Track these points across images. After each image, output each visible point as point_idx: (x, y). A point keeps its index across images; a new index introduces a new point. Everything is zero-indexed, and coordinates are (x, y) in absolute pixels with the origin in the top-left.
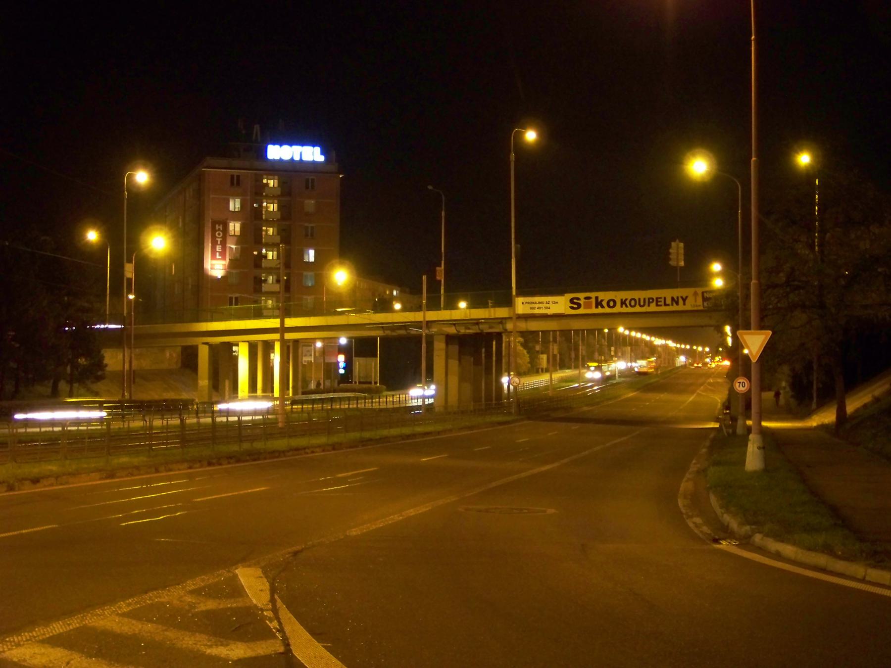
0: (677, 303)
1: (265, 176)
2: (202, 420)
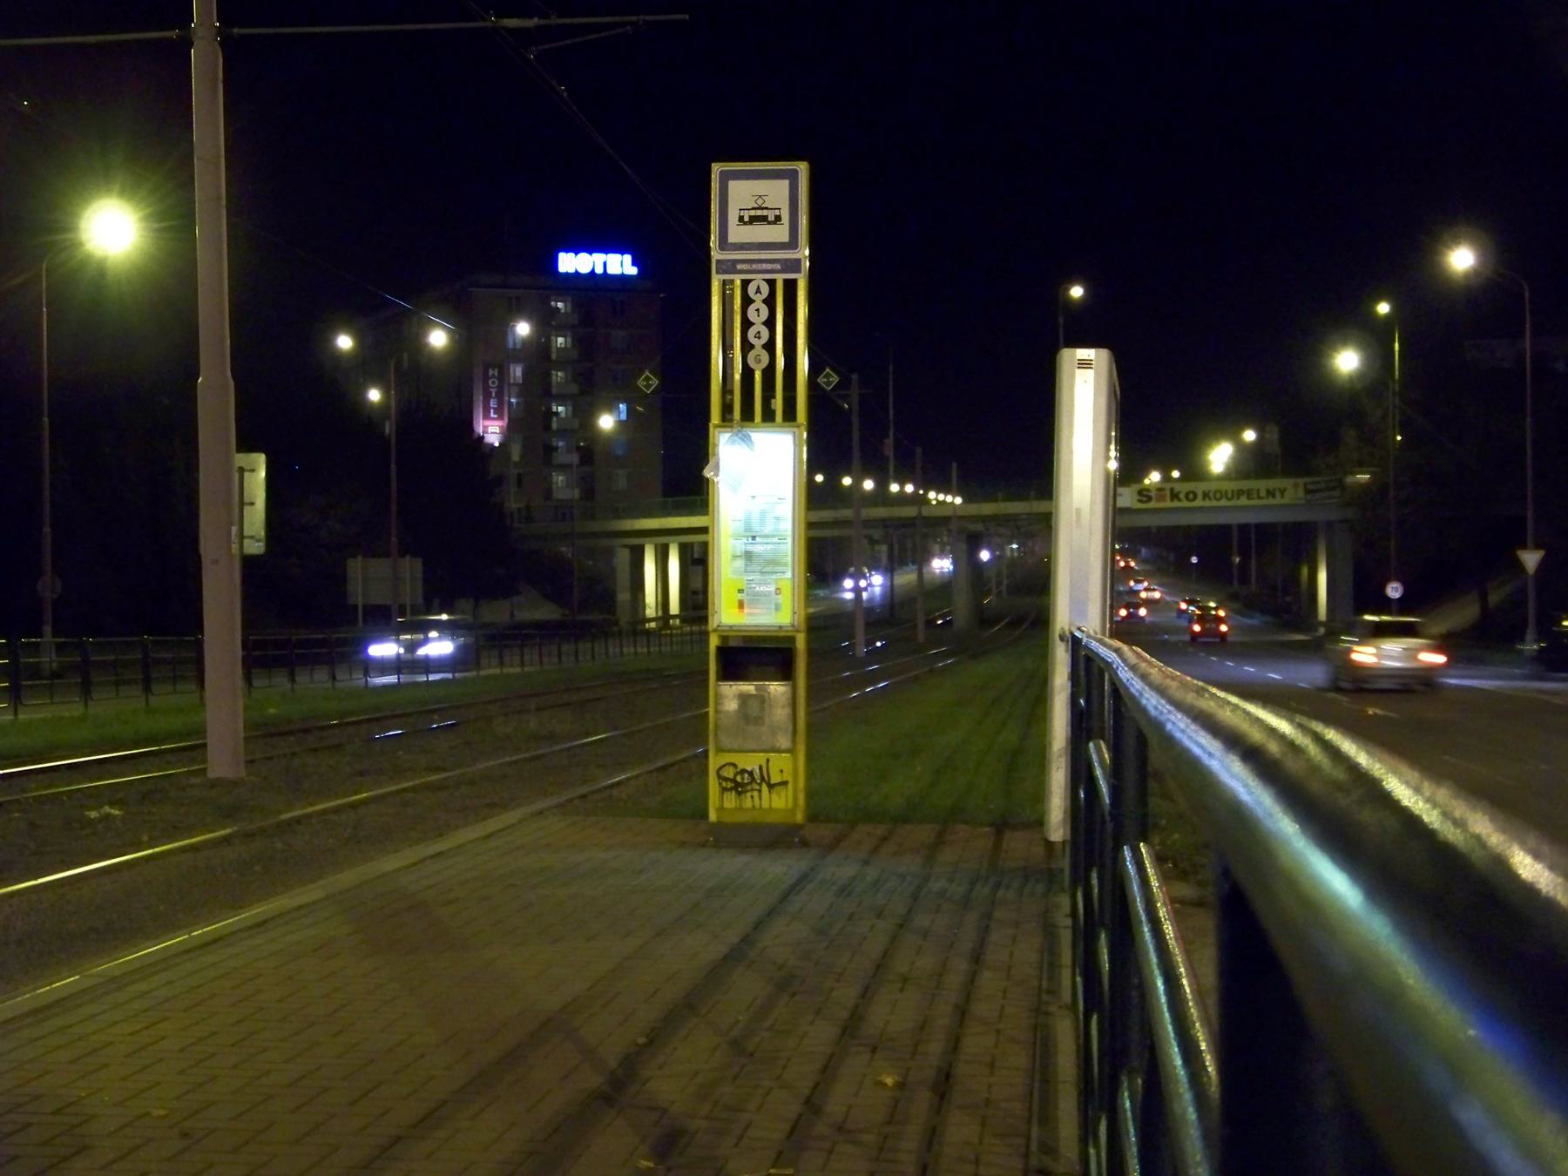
0: (1274, 496)
1: (553, 297)
2: (689, 629)
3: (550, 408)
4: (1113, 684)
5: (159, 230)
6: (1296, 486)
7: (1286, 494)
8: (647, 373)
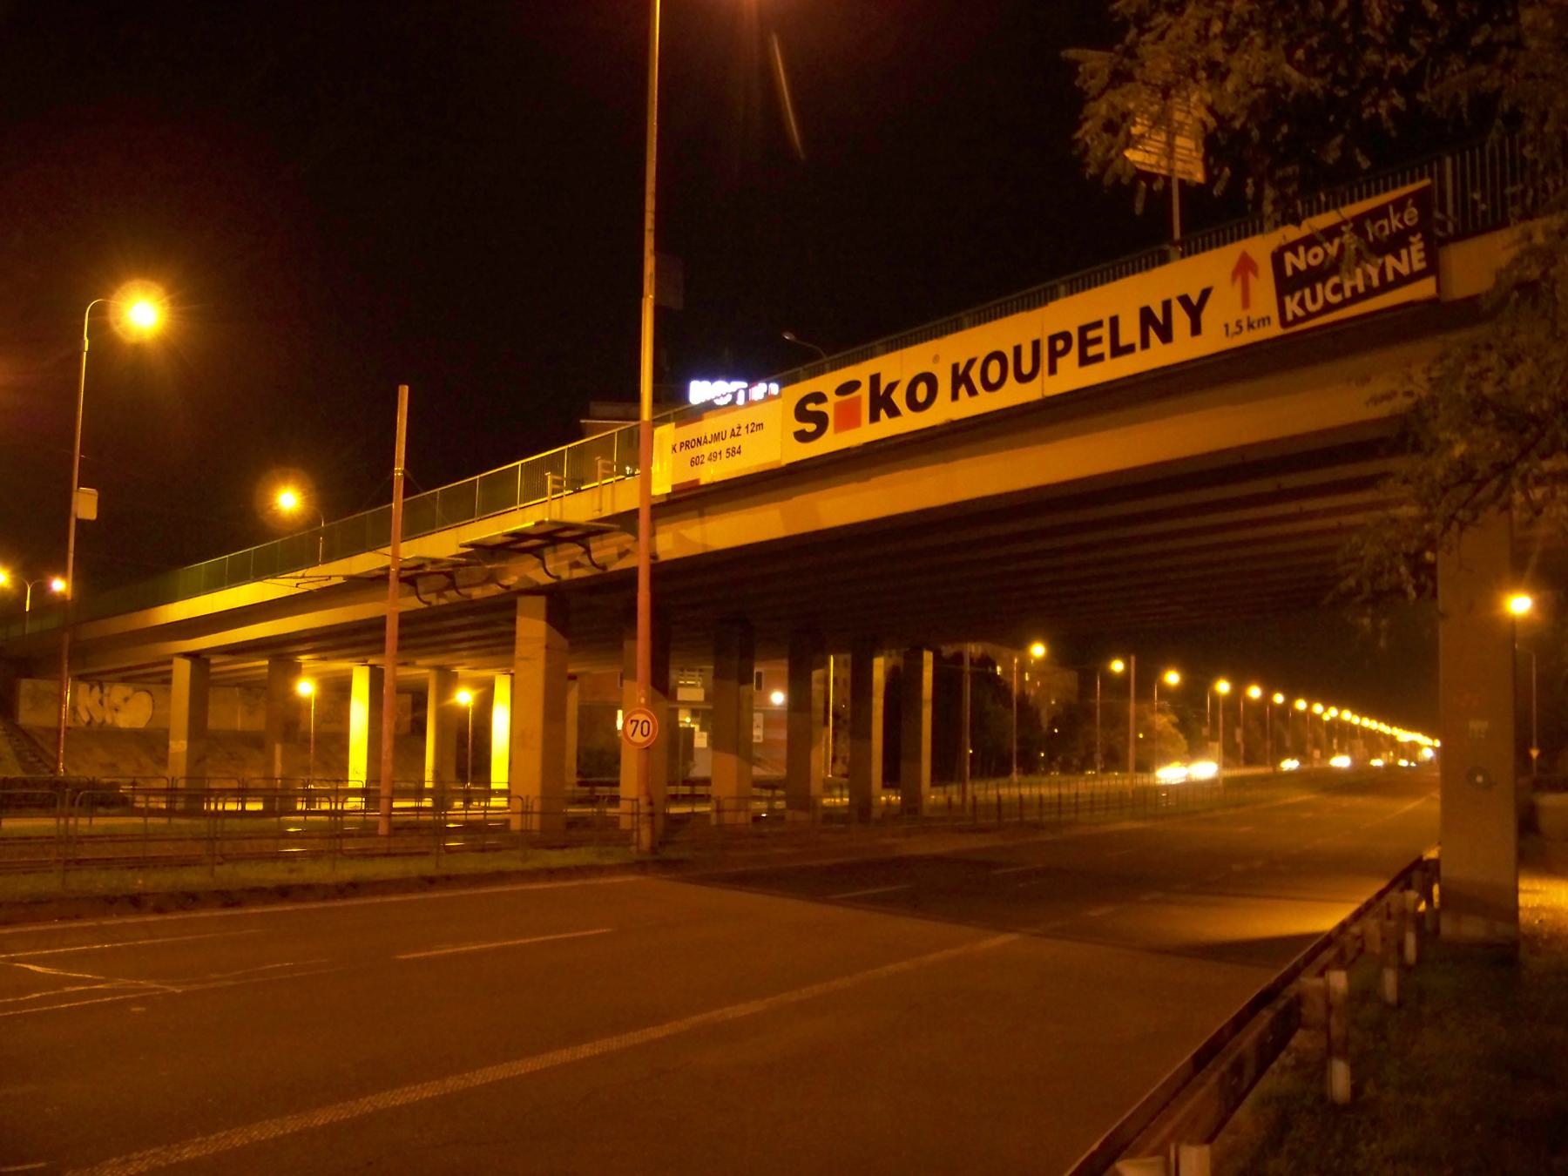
0: (1166, 335)
4: (449, 567)
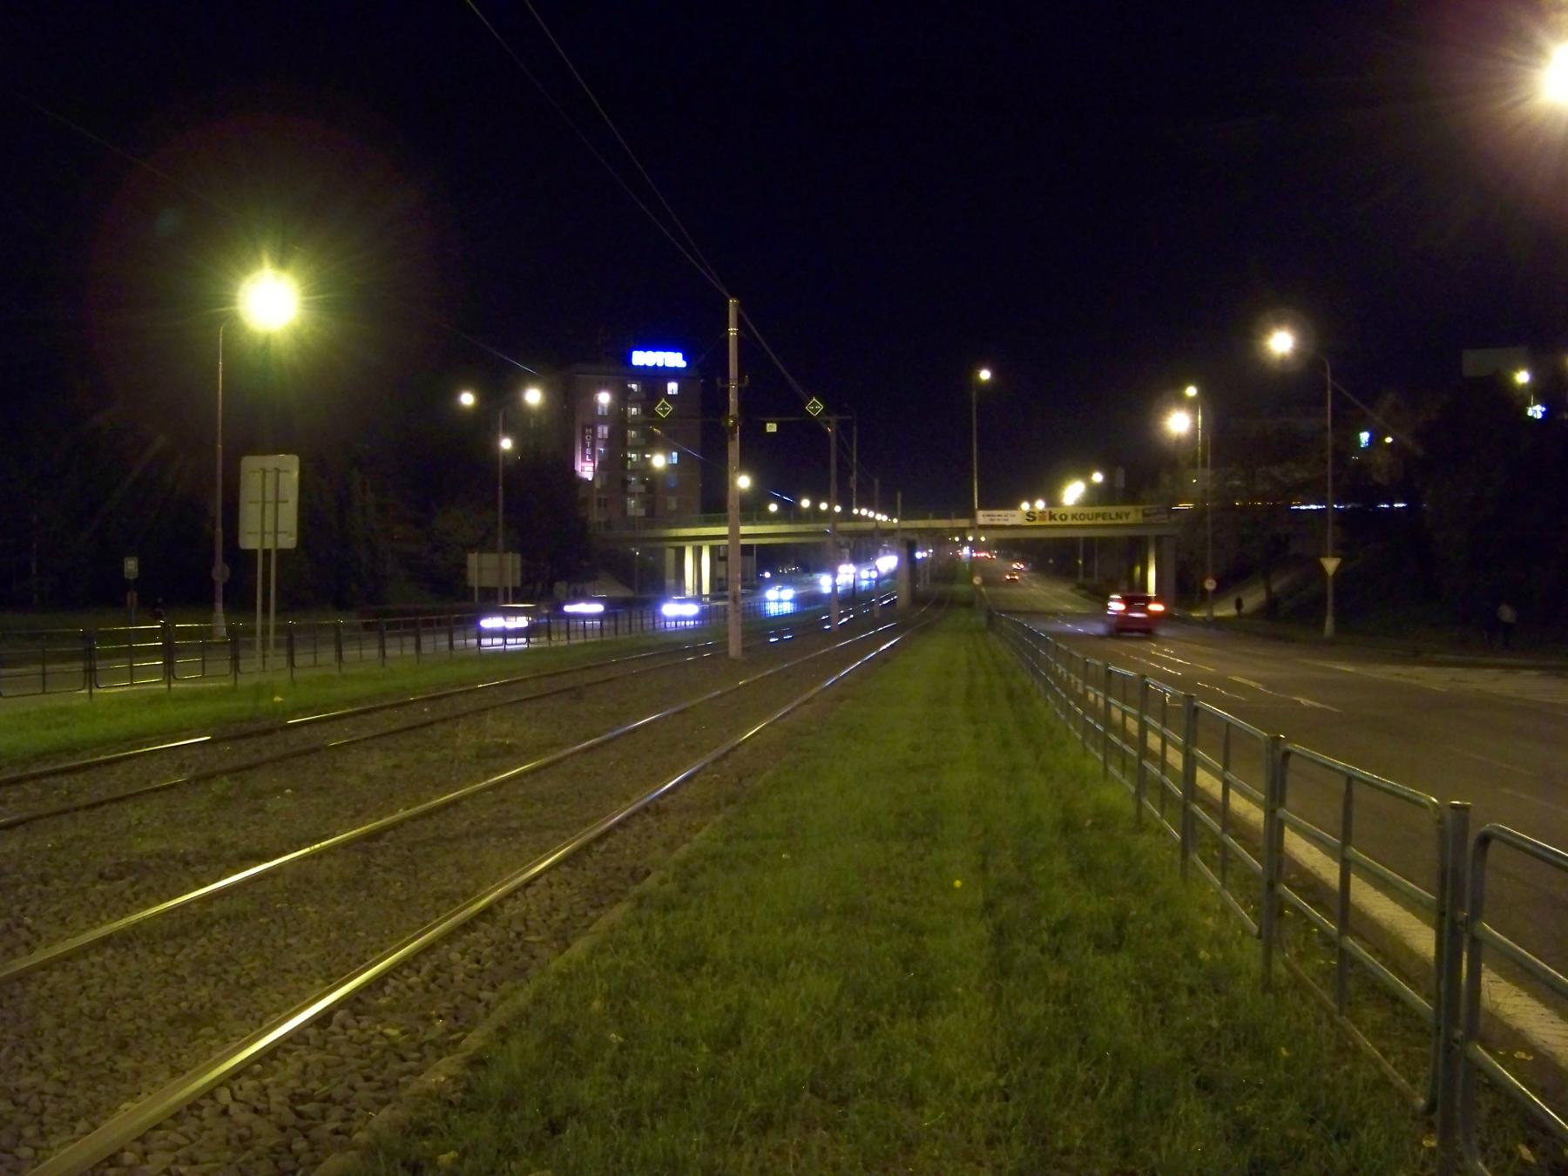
0: (1117, 514)
3: (626, 455)
5: (307, 302)
6: (1137, 511)
7: (1130, 516)
8: (663, 401)
